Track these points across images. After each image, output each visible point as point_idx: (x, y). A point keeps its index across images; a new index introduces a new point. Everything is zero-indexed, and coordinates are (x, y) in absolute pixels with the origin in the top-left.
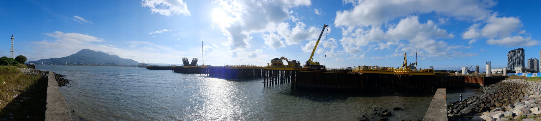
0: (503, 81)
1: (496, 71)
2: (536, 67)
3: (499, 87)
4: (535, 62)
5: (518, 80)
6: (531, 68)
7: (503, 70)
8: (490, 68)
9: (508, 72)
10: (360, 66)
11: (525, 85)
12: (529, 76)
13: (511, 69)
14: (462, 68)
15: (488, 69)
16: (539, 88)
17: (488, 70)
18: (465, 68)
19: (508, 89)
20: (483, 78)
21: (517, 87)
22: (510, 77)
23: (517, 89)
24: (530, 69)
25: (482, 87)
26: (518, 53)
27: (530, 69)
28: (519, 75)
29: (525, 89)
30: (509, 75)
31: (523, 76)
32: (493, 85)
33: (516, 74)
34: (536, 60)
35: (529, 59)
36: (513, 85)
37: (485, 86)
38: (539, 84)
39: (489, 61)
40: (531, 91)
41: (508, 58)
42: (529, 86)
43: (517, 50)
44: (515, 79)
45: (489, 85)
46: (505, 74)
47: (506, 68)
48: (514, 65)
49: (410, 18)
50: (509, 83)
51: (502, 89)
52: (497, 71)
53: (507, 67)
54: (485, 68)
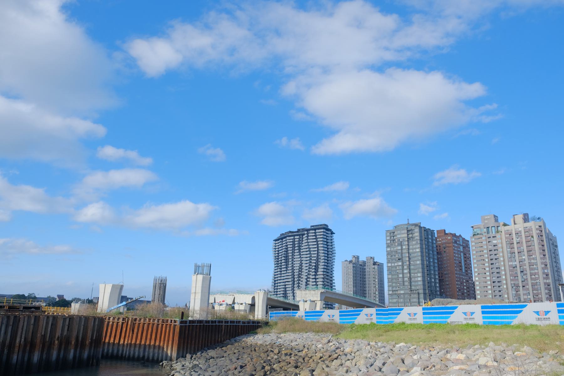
0: (251, 340)
1: (230, 302)
2: (373, 289)
3: (234, 360)
4: (370, 270)
5: (305, 335)
6: (355, 293)
7: (253, 298)
8: (207, 290)
9: (272, 305)
10: (367, 314)
11: (327, 354)
12: (347, 320)
13: (285, 296)
14: (102, 286)
15: (199, 290)
16: (378, 364)
17: (199, 296)
18: (114, 286)
19: (263, 367)
20: (178, 323)
21: (301, 360)
22: (276, 324)
23: (296, 367)
24: (351, 294)
25: (171, 360)
26: (308, 242)
27: (351, 294)
28: (310, 319)
29: (327, 369)
30: (276, 316)
31: (325, 323)
32: (212, 353)
33: (300, 313)
34: (375, 263)
35: (351, 262)
36: (286, 354)
37: (181, 355)
38: (382, 350)
39: (207, 262)
40: (347, 372)
41: (277, 258)
42: (344, 357)
43: (308, 230)
44: (294, 331)
45: (199, 354)
46: (259, 314)
47: (267, 292)
48: (296, 283)
49: (535, 216)
50: (272, 345)
51: (242, 367)
52: (234, 303)
53: (271, 289)
54: (188, 293)
